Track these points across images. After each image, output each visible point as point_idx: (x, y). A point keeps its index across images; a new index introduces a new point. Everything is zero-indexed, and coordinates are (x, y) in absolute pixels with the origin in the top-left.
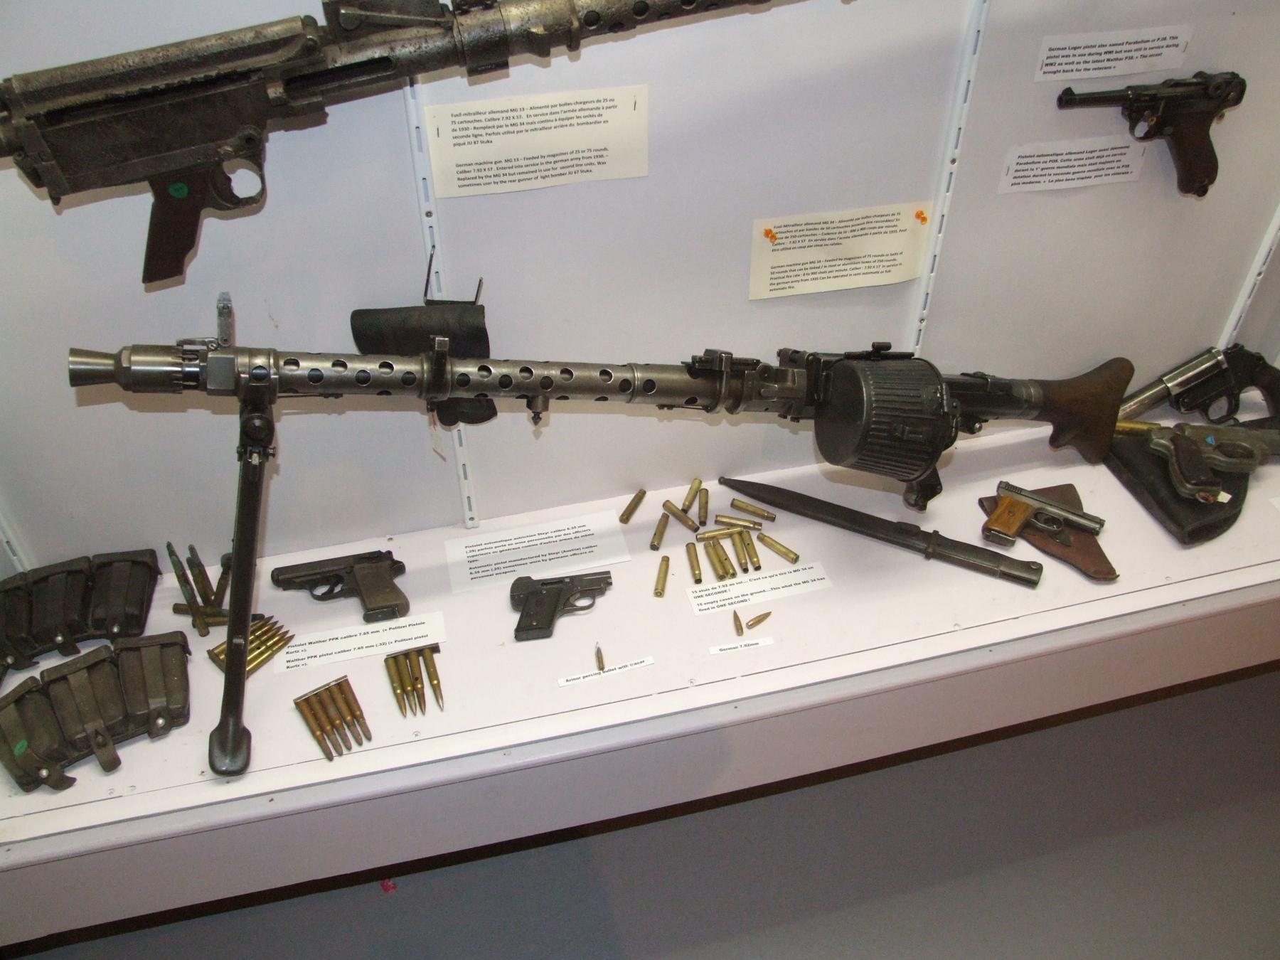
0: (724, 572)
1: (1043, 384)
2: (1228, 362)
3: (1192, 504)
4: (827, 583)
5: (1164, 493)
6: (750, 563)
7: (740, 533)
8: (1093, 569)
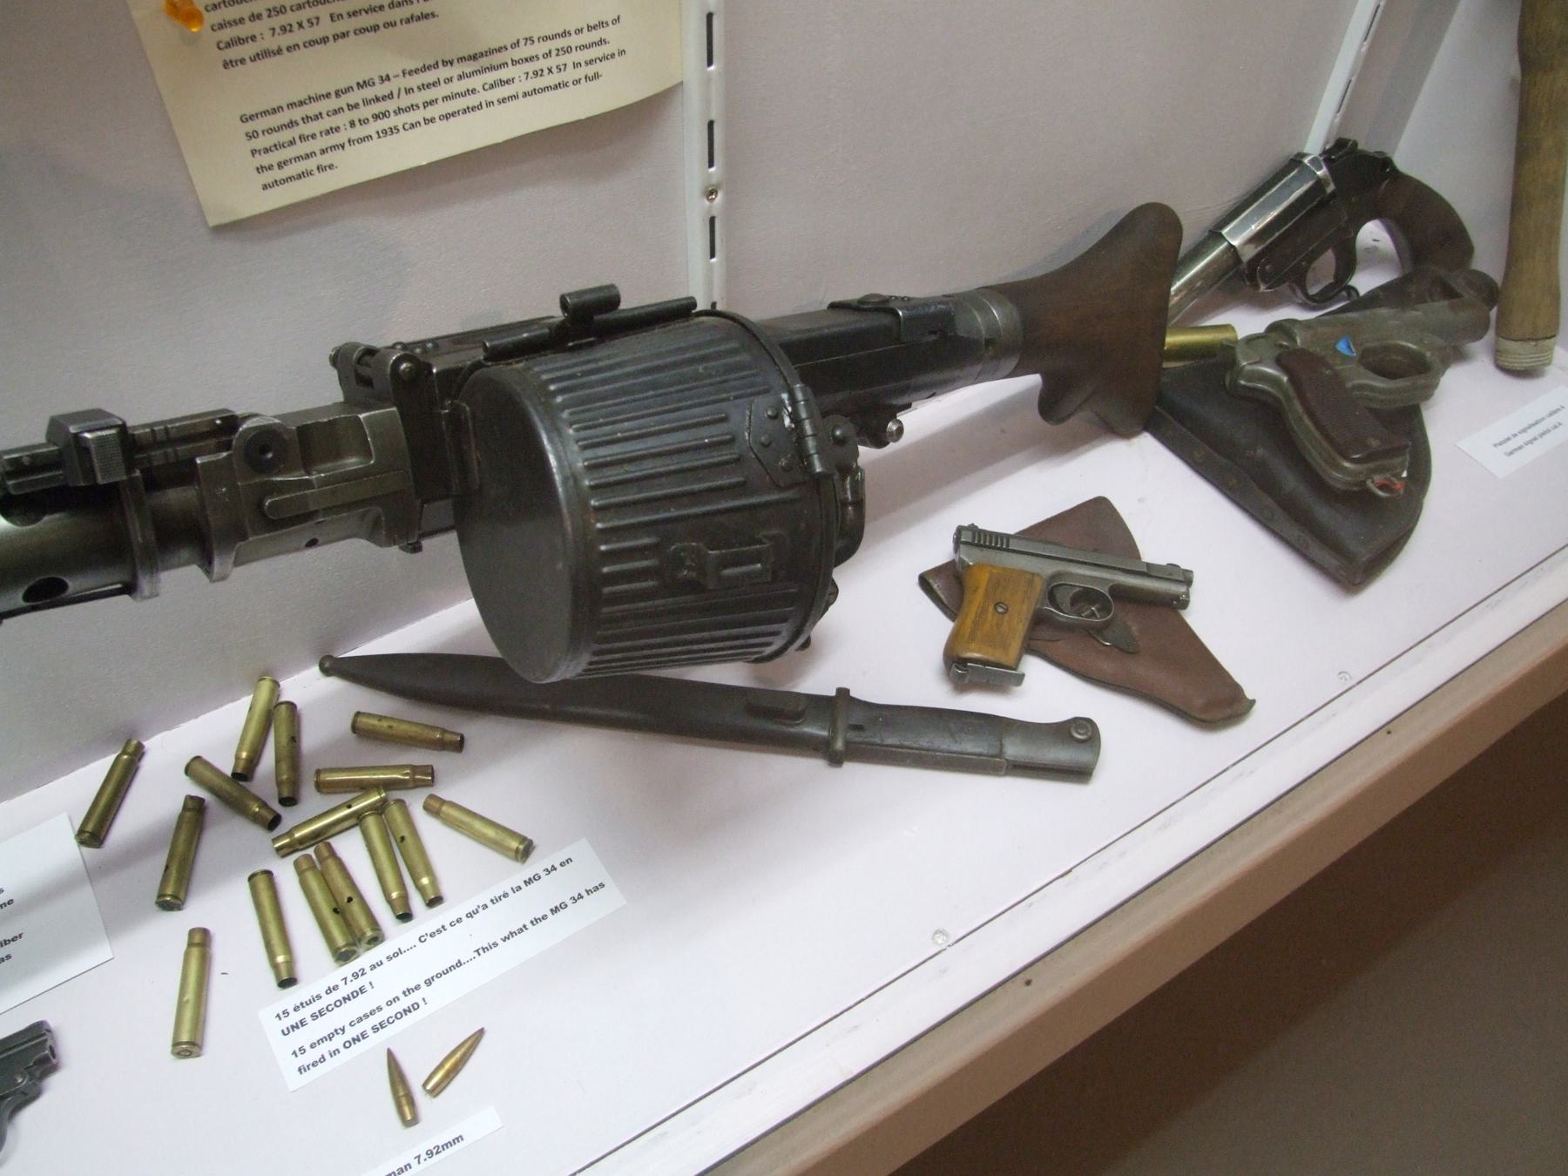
0: (351, 932)
1: (1009, 292)
2: (1335, 180)
3: (1338, 490)
4: (610, 900)
5: (1291, 482)
6: (413, 889)
7: (379, 809)
8: (1199, 702)
